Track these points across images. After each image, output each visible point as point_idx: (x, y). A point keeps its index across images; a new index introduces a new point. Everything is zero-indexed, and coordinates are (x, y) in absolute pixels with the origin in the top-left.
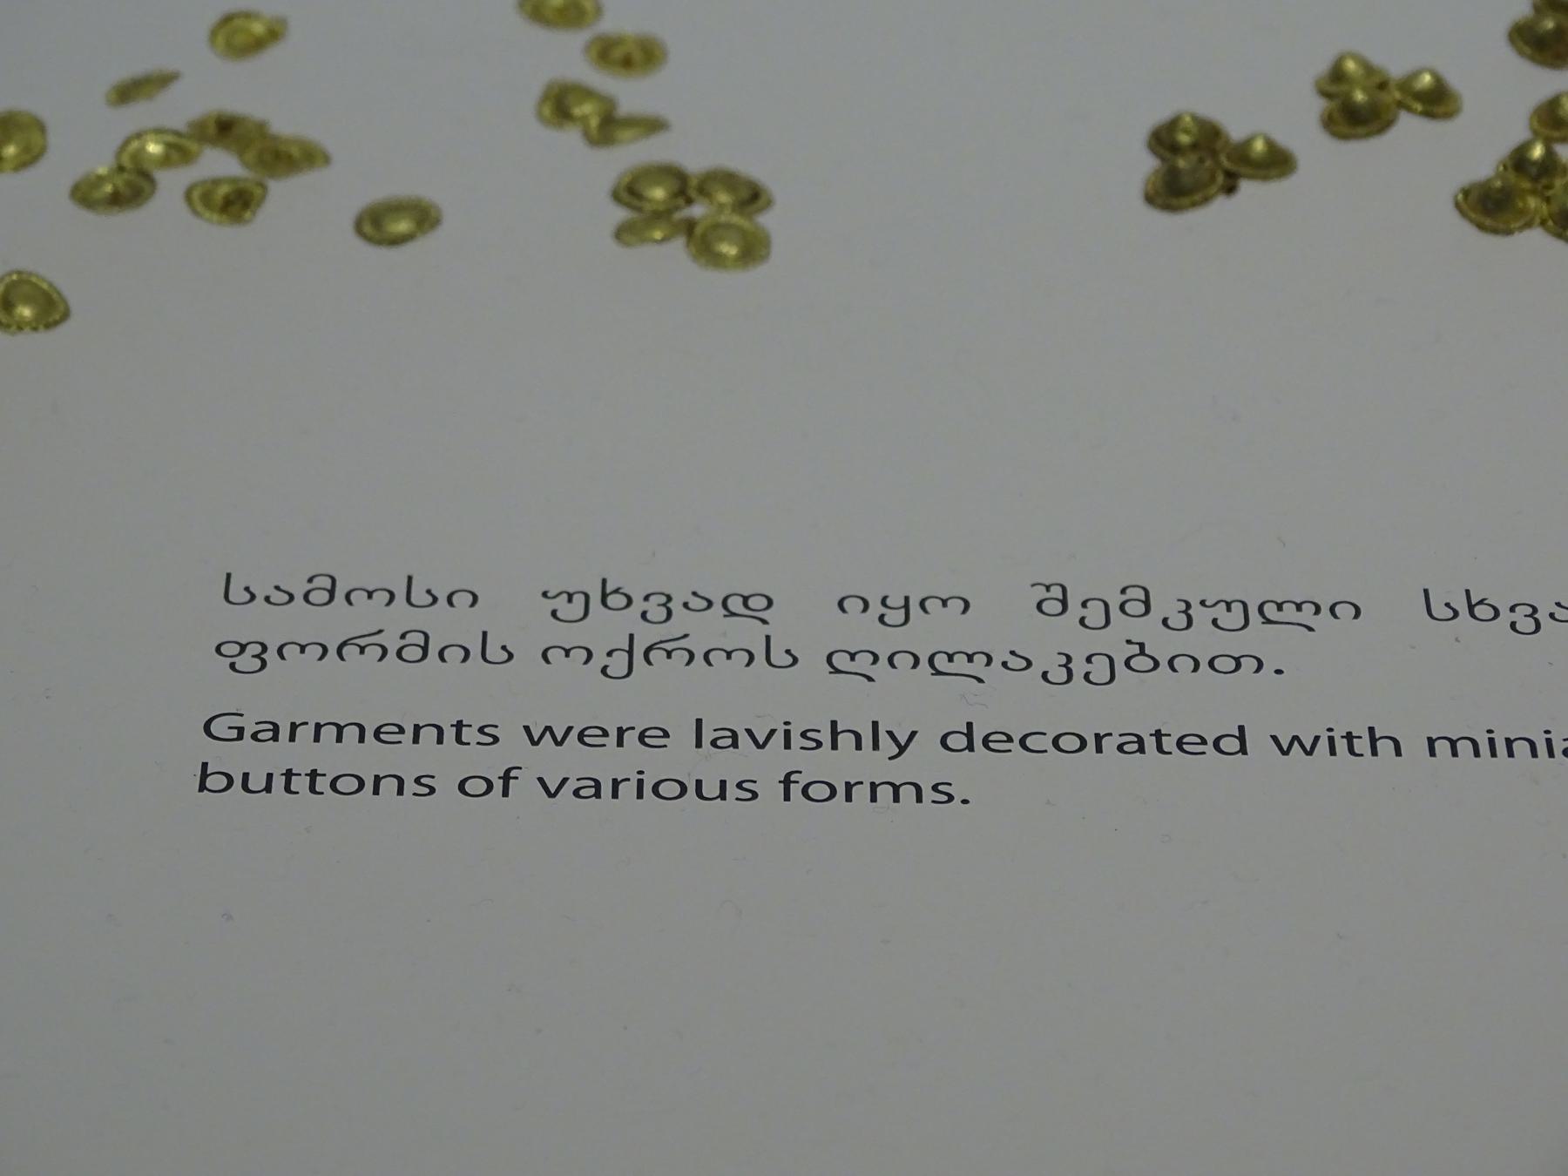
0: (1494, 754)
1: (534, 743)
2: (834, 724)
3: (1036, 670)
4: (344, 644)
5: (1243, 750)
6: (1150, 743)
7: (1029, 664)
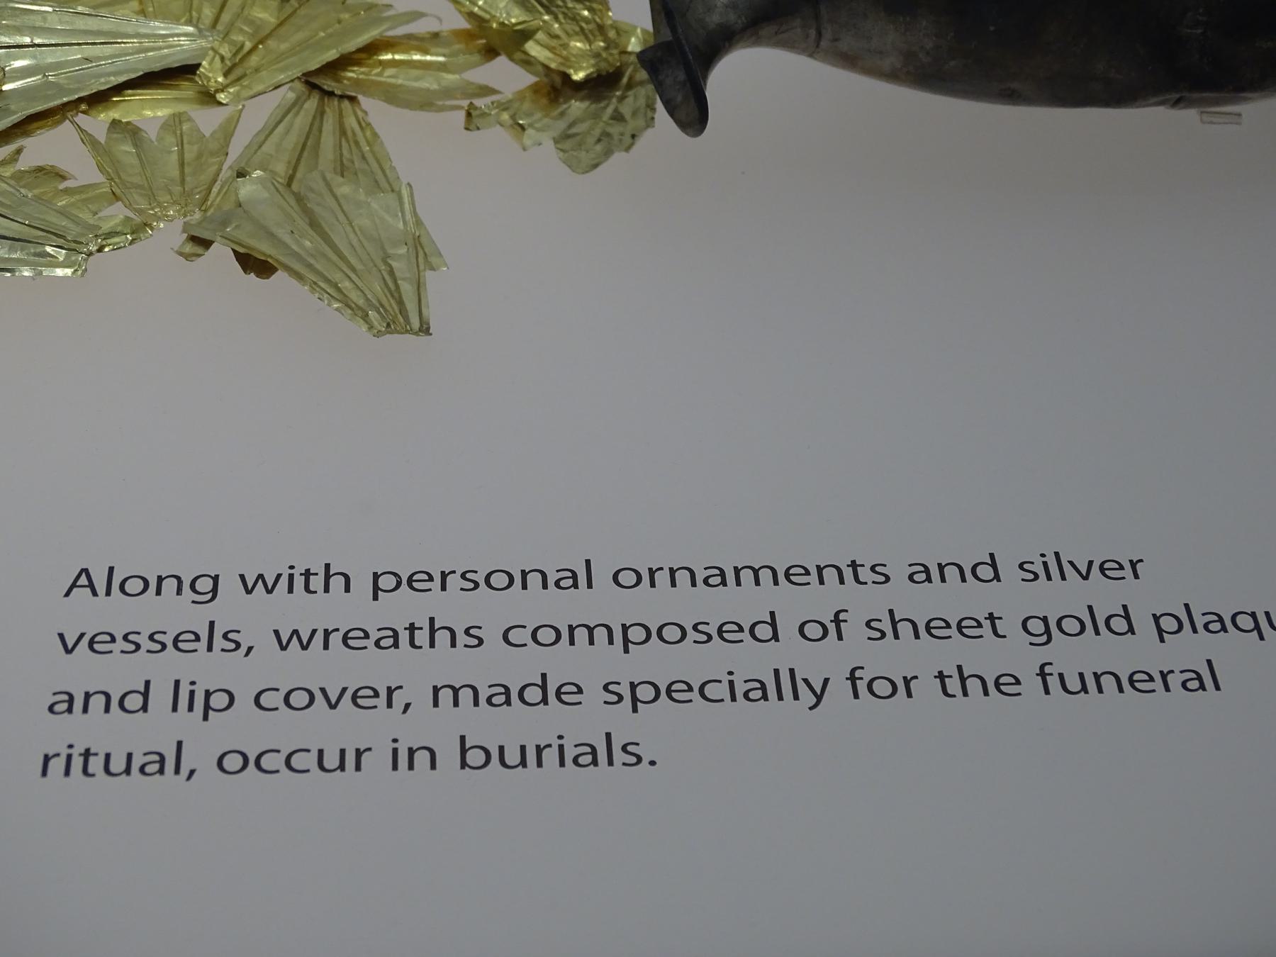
0: (780, 698)
5: (775, 637)
6: (404, 637)
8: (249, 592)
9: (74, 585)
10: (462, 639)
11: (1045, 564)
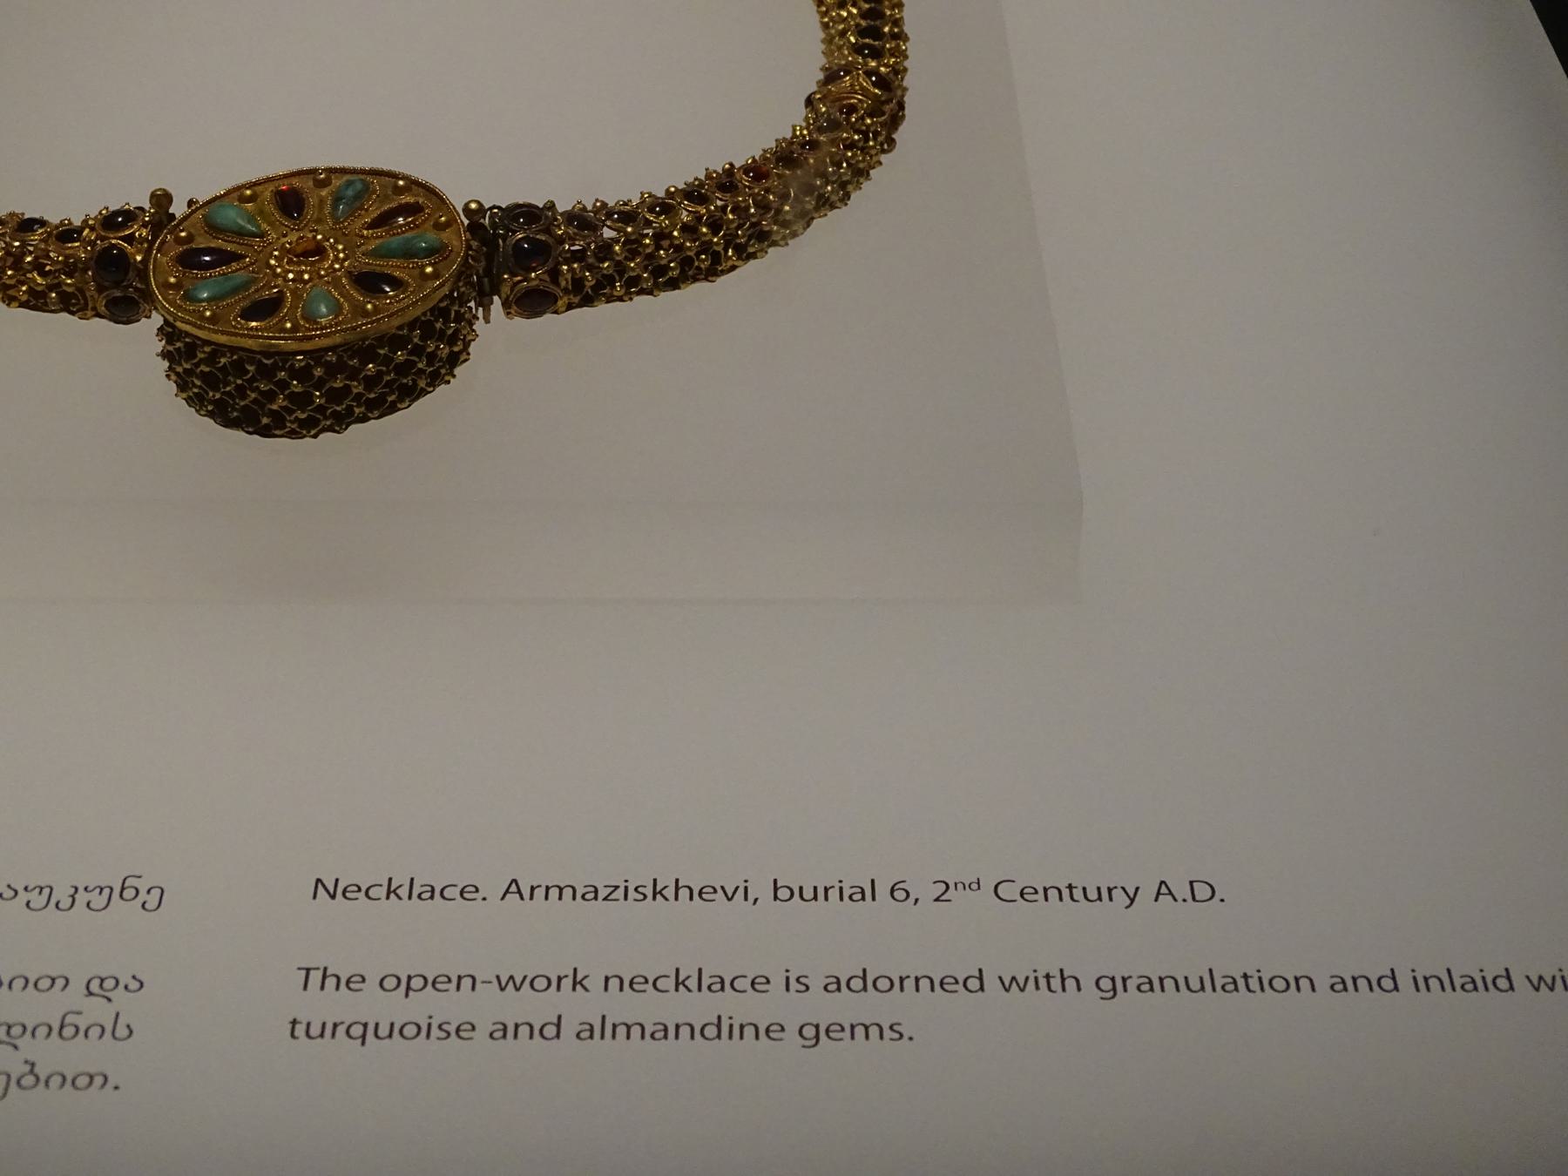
1: (1007, 990)
5: (982, 988)
8: (502, 989)
9: (507, 891)
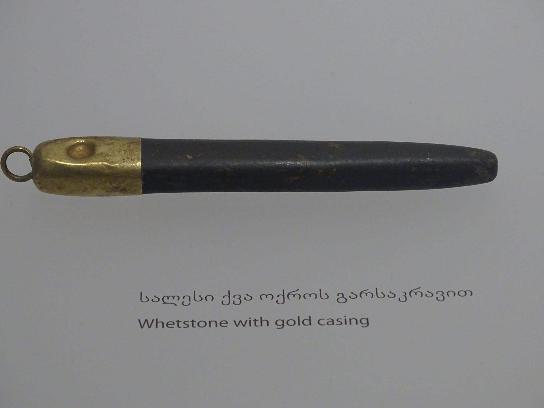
1: (237, 326)
2: (261, 318)
3: (397, 298)
4: (361, 293)
5: (310, 324)
7: (395, 295)
8: (237, 326)
10: (336, 322)
11: (345, 320)
